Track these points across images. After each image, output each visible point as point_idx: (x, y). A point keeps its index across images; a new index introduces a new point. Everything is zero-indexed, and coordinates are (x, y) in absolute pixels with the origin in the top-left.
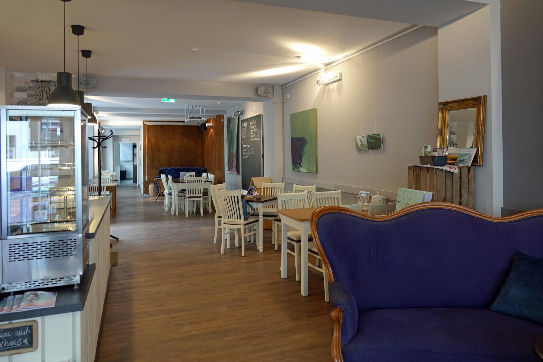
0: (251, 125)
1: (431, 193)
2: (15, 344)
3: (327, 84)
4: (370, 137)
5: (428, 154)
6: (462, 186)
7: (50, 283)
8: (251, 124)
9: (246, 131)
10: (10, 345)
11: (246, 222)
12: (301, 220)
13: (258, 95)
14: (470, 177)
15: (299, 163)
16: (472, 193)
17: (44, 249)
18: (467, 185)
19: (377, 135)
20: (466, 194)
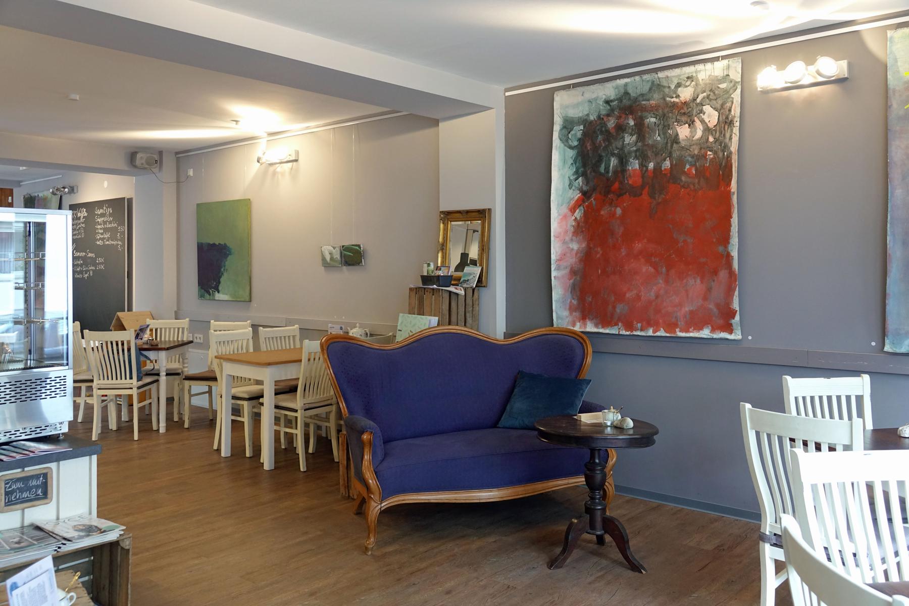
0: (98, 215)
1: (437, 318)
2: (29, 496)
3: (271, 164)
4: (344, 249)
5: (430, 273)
6: (466, 309)
7: (23, 435)
8: (99, 213)
9: (83, 225)
10: (23, 497)
11: (140, 383)
12: (266, 363)
13: (135, 166)
14: (474, 299)
15: (213, 286)
16: (476, 318)
17: (8, 391)
18: (472, 308)
19: (356, 245)
20: (471, 318)
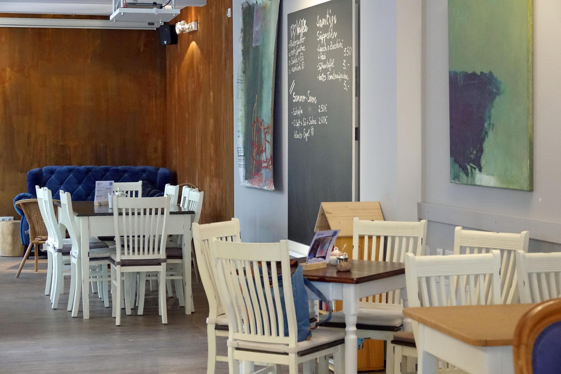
9: (303, 48)
11: (305, 345)
15: (472, 156)
